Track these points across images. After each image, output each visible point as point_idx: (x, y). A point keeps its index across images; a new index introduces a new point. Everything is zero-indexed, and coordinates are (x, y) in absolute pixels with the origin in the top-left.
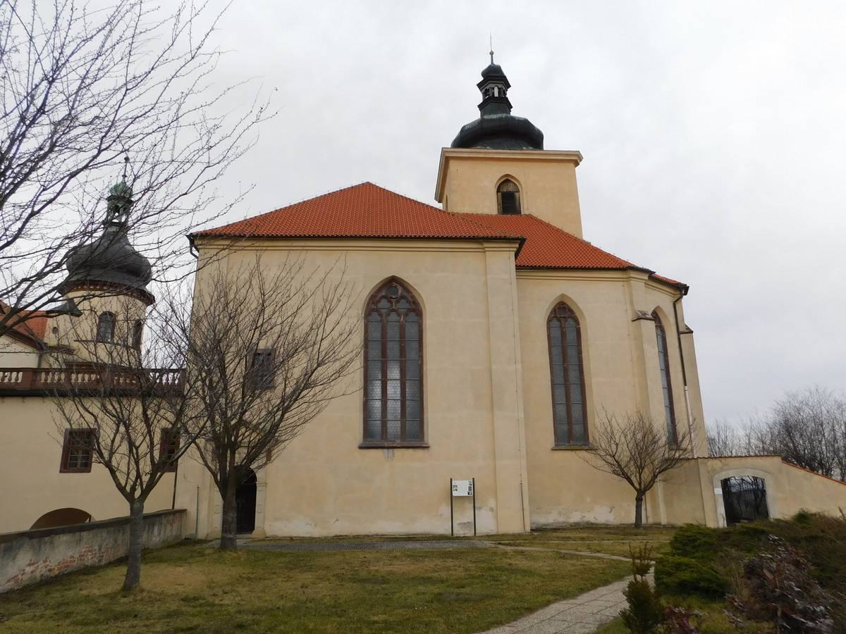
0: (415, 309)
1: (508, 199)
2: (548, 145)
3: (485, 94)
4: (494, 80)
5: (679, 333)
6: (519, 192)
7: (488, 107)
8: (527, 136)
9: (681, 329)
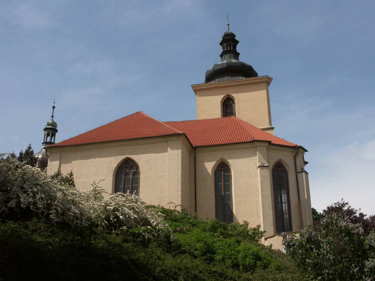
0: (137, 173)
1: (228, 106)
2: (260, 75)
3: (224, 48)
4: (229, 43)
5: (297, 173)
6: (235, 103)
7: (223, 57)
8: (247, 72)
9: (299, 170)
